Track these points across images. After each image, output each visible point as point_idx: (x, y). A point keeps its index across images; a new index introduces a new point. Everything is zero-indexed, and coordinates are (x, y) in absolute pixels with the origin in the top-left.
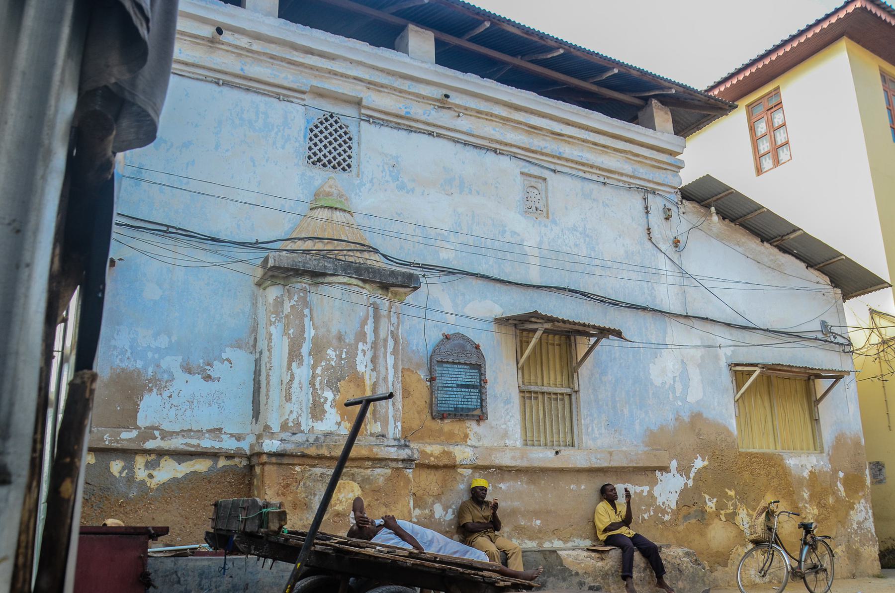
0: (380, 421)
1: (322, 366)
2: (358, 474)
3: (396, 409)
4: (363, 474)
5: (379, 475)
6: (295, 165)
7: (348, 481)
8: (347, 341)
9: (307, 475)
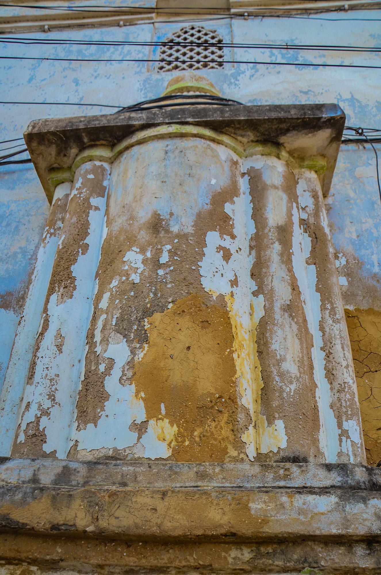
0: (284, 418)
1: (111, 290)
6: (136, 74)
8: (175, 229)
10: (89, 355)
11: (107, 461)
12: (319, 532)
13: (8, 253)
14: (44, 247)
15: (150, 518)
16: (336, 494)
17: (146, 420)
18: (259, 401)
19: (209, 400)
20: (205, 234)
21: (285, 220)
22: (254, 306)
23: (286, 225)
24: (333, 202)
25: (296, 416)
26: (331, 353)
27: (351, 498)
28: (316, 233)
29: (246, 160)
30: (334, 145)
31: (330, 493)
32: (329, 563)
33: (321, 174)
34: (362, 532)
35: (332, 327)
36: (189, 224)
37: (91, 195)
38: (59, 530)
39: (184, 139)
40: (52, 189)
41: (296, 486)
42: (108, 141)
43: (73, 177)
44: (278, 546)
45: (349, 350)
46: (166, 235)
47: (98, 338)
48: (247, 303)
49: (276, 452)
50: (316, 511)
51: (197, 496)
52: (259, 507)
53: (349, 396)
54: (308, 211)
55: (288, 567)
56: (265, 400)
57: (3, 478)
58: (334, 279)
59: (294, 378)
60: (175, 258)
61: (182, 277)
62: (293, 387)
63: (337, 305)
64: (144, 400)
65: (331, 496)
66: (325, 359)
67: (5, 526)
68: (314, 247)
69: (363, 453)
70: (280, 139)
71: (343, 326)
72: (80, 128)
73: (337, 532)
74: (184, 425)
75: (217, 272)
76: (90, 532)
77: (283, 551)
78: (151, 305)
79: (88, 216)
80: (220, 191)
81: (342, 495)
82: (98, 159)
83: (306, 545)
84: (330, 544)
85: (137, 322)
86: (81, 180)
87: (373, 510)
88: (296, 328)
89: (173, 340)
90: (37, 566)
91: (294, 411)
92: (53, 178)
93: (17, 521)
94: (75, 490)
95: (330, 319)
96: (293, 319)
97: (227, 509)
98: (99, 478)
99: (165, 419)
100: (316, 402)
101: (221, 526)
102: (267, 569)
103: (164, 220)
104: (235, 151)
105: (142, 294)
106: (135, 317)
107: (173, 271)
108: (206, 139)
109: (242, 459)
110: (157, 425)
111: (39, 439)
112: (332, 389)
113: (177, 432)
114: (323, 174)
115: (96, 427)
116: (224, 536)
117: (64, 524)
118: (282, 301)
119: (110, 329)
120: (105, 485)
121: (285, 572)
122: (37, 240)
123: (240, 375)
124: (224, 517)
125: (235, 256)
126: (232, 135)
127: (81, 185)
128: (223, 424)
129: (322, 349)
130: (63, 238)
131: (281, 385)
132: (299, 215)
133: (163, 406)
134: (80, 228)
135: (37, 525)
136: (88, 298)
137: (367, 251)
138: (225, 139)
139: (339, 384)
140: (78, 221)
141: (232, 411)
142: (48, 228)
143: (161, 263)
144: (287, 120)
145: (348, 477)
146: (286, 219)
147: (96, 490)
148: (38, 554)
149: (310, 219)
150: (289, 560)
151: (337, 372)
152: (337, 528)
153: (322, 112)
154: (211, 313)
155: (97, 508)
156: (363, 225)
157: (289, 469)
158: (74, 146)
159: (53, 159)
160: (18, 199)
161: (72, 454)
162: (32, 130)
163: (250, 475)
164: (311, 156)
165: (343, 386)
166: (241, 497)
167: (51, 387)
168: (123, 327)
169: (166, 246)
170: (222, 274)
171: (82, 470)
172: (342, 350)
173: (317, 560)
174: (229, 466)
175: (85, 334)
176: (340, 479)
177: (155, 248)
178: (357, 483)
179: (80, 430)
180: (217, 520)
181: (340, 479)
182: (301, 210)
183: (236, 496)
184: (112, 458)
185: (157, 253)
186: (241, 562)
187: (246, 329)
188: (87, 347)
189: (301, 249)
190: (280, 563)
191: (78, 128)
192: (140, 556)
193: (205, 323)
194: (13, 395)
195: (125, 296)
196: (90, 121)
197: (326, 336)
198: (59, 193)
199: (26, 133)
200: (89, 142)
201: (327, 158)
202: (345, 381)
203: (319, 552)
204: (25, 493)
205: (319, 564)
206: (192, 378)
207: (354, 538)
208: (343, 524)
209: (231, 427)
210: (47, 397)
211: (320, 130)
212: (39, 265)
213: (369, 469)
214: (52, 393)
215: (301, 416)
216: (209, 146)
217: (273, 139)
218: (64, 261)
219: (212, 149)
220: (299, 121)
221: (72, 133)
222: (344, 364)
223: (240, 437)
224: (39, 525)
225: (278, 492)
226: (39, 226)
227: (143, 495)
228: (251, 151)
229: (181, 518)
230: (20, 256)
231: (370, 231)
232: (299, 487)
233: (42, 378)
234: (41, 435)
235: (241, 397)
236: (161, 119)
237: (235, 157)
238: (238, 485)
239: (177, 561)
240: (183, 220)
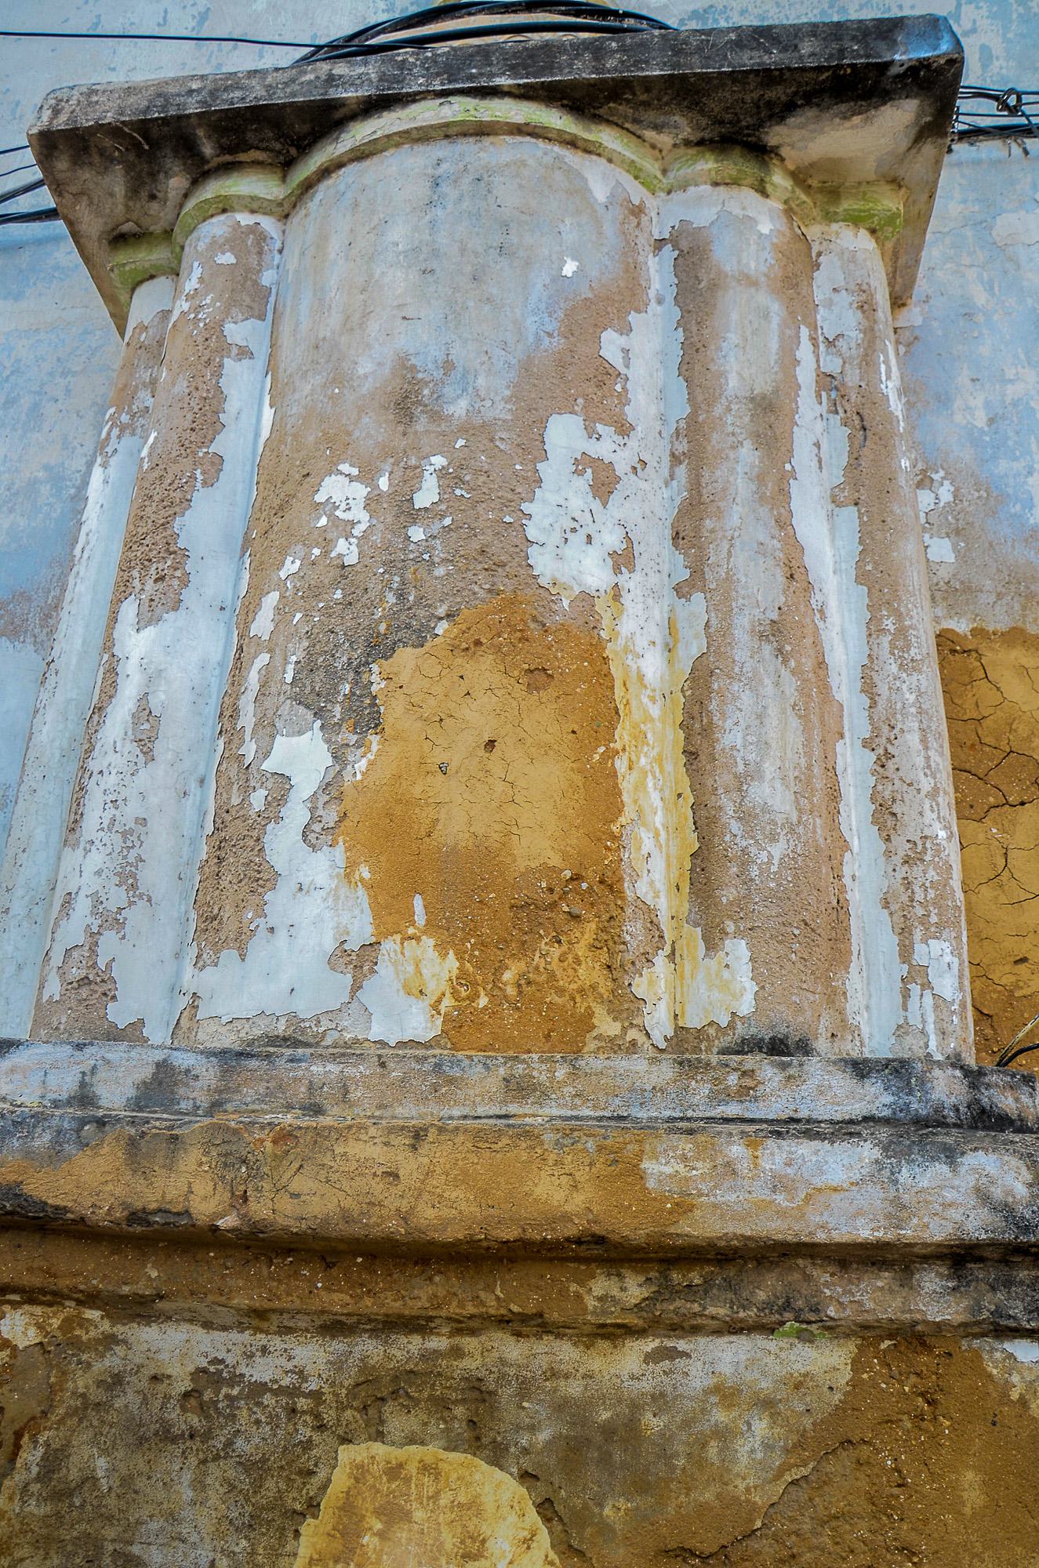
1: (281, 585)
2: (525, 1389)
3: (902, 847)
4: (574, 1389)
5: (726, 1393)
7: (431, 1451)
8: (459, 408)
9: (82, 1382)
10: (225, 765)
11: (272, 1050)
12: (824, 1236)
13: (13, 484)
14: (105, 466)
15: (381, 1197)
16: (876, 1138)
17: (373, 940)
18: (686, 888)
19: (544, 885)
20: (543, 423)
21: (773, 376)
22: (679, 626)
23: (776, 391)
24: (924, 320)
25: (783, 929)
26: (889, 756)
27: (916, 1149)
28: (865, 413)
29: (668, 201)
30: (928, 149)
31: (859, 1134)
32: (848, 1312)
33: (887, 238)
34: (938, 1238)
35: (898, 684)
36: (496, 393)
37: (227, 312)
38: (149, 1224)
39: (487, 141)
40: (123, 297)
41: (771, 1117)
42: (272, 151)
43: (180, 262)
44: (717, 1270)
45: (941, 746)
46: (433, 427)
47: (247, 719)
48: (659, 613)
49: (724, 1024)
50: (818, 1182)
51: (505, 1141)
52: (668, 1170)
53: (933, 873)
54: (844, 349)
55: (742, 1321)
56: (700, 886)
57: (3, 1093)
58: (910, 548)
59: (783, 824)
60: (458, 492)
61: (475, 545)
62: (778, 850)
63: (914, 621)
64: (370, 887)
65: (862, 1143)
66: (874, 772)
67: (11, 1213)
68: (855, 455)
69: (965, 1028)
70: (767, 133)
71: (929, 679)
72: (187, 112)
73: (872, 1235)
74: (477, 953)
75: (574, 530)
76: (228, 1231)
77: (730, 1282)
78: (389, 626)
79: (220, 376)
80: (590, 295)
81: (891, 1142)
82: (246, 207)
83: (790, 1269)
84: (855, 1266)
85: (351, 675)
86: (197, 272)
87: (971, 1180)
88: (794, 686)
89: (448, 722)
90: (99, 1308)
91: (779, 915)
92: (124, 265)
93: (42, 1202)
94: (185, 1123)
95: (892, 661)
96: (785, 662)
97: (582, 1175)
98: (249, 1093)
99: (424, 938)
100: (843, 889)
101: (566, 1218)
102: (685, 1325)
103: (427, 383)
104: (637, 173)
105: (366, 597)
106: (345, 659)
107: (451, 530)
108: (550, 140)
109: (634, 1043)
110: (402, 953)
111: (96, 992)
112: (888, 854)
113: (455, 972)
114: (894, 239)
115: (243, 960)
116: (575, 1243)
117: (160, 1210)
118: (756, 612)
119: (279, 694)
120: (266, 1112)
121: (735, 1333)
122: (89, 447)
123: (634, 816)
124: (575, 1195)
125: (629, 483)
126: (627, 125)
127: (197, 286)
128: (581, 950)
129: (867, 744)
130: (151, 440)
131: (744, 843)
132: (818, 361)
133: (418, 902)
134: (196, 410)
135: (92, 1213)
136: (222, 609)
137: (1015, 465)
138: (607, 137)
139: (908, 841)
140: (192, 389)
141: (608, 915)
142: (112, 410)
143: (416, 507)
144: (787, 75)
145: (910, 1093)
146: (776, 373)
147: (241, 1126)
148: (100, 1282)
149: (849, 372)
150: (746, 1303)
151: (905, 809)
152: (872, 1225)
153: (893, 45)
154: (555, 645)
155: (244, 1169)
156: (1009, 386)
157: (753, 1071)
158: (176, 169)
159: (120, 208)
160: (34, 328)
161: (185, 1029)
162: (51, 120)
163: (649, 1087)
164: (860, 183)
165: (920, 848)
166: (622, 1146)
167: (125, 853)
168: (313, 689)
169: (433, 459)
170: (589, 537)
171: (205, 1074)
172: (921, 747)
173: (818, 1304)
174: (592, 1063)
175: (212, 709)
176: (888, 1099)
177: (402, 464)
178: (936, 1111)
179: (204, 967)
180: (556, 1204)
181: (888, 1099)
182: (822, 347)
183: (609, 1142)
184: (286, 1041)
185: (406, 478)
186: (618, 1308)
187: (654, 690)
188: (221, 742)
189: (820, 461)
190: (722, 1311)
191: (181, 112)
192: (359, 1291)
193: (538, 676)
194: (34, 869)
195: (320, 601)
196: (217, 90)
197: (879, 707)
198: (144, 305)
199: (35, 131)
200: (218, 156)
201: (907, 188)
202: (927, 832)
203: (824, 1285)
204: (59, 1132)
205: (822, 1315)
206: (497, 827)
207: (916, 1250)
208: (889, 1216)
209: (604, 957)
210: (117, 880)
211: (884, 103)
212: (92, 515)
213: (972, 1072)
214: (128, 868)
215: (797, 928)
216: (559, 163)
217: (749, 135)
218: (154, 504)
219: (569, 171)
220: (824, 77)
221: (166, 129)
222: (926, 785)
223: (630, 984)
224: (97, 1211)
225: (719, 1133)
226: (95, 404)
227: (363, 1137)
228: (682, 172)
229: (462, 1196)
230: (45, 490)
231: (1028, 403)
232: (777, 1121)
233: (102, 829)
234: (103, 981)
235: (636, 877)
236: (421, 80)
237: (637, 193)
238: (615, 1114)
239: (455, 1304)
240: (481, 381)
